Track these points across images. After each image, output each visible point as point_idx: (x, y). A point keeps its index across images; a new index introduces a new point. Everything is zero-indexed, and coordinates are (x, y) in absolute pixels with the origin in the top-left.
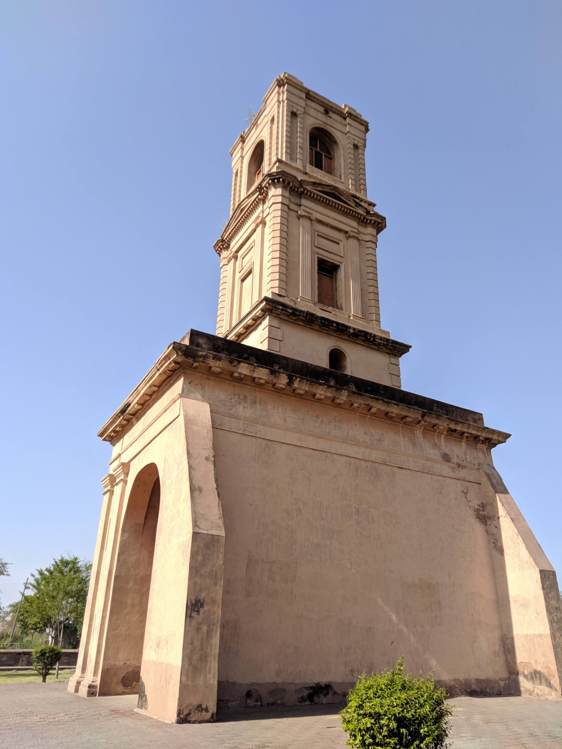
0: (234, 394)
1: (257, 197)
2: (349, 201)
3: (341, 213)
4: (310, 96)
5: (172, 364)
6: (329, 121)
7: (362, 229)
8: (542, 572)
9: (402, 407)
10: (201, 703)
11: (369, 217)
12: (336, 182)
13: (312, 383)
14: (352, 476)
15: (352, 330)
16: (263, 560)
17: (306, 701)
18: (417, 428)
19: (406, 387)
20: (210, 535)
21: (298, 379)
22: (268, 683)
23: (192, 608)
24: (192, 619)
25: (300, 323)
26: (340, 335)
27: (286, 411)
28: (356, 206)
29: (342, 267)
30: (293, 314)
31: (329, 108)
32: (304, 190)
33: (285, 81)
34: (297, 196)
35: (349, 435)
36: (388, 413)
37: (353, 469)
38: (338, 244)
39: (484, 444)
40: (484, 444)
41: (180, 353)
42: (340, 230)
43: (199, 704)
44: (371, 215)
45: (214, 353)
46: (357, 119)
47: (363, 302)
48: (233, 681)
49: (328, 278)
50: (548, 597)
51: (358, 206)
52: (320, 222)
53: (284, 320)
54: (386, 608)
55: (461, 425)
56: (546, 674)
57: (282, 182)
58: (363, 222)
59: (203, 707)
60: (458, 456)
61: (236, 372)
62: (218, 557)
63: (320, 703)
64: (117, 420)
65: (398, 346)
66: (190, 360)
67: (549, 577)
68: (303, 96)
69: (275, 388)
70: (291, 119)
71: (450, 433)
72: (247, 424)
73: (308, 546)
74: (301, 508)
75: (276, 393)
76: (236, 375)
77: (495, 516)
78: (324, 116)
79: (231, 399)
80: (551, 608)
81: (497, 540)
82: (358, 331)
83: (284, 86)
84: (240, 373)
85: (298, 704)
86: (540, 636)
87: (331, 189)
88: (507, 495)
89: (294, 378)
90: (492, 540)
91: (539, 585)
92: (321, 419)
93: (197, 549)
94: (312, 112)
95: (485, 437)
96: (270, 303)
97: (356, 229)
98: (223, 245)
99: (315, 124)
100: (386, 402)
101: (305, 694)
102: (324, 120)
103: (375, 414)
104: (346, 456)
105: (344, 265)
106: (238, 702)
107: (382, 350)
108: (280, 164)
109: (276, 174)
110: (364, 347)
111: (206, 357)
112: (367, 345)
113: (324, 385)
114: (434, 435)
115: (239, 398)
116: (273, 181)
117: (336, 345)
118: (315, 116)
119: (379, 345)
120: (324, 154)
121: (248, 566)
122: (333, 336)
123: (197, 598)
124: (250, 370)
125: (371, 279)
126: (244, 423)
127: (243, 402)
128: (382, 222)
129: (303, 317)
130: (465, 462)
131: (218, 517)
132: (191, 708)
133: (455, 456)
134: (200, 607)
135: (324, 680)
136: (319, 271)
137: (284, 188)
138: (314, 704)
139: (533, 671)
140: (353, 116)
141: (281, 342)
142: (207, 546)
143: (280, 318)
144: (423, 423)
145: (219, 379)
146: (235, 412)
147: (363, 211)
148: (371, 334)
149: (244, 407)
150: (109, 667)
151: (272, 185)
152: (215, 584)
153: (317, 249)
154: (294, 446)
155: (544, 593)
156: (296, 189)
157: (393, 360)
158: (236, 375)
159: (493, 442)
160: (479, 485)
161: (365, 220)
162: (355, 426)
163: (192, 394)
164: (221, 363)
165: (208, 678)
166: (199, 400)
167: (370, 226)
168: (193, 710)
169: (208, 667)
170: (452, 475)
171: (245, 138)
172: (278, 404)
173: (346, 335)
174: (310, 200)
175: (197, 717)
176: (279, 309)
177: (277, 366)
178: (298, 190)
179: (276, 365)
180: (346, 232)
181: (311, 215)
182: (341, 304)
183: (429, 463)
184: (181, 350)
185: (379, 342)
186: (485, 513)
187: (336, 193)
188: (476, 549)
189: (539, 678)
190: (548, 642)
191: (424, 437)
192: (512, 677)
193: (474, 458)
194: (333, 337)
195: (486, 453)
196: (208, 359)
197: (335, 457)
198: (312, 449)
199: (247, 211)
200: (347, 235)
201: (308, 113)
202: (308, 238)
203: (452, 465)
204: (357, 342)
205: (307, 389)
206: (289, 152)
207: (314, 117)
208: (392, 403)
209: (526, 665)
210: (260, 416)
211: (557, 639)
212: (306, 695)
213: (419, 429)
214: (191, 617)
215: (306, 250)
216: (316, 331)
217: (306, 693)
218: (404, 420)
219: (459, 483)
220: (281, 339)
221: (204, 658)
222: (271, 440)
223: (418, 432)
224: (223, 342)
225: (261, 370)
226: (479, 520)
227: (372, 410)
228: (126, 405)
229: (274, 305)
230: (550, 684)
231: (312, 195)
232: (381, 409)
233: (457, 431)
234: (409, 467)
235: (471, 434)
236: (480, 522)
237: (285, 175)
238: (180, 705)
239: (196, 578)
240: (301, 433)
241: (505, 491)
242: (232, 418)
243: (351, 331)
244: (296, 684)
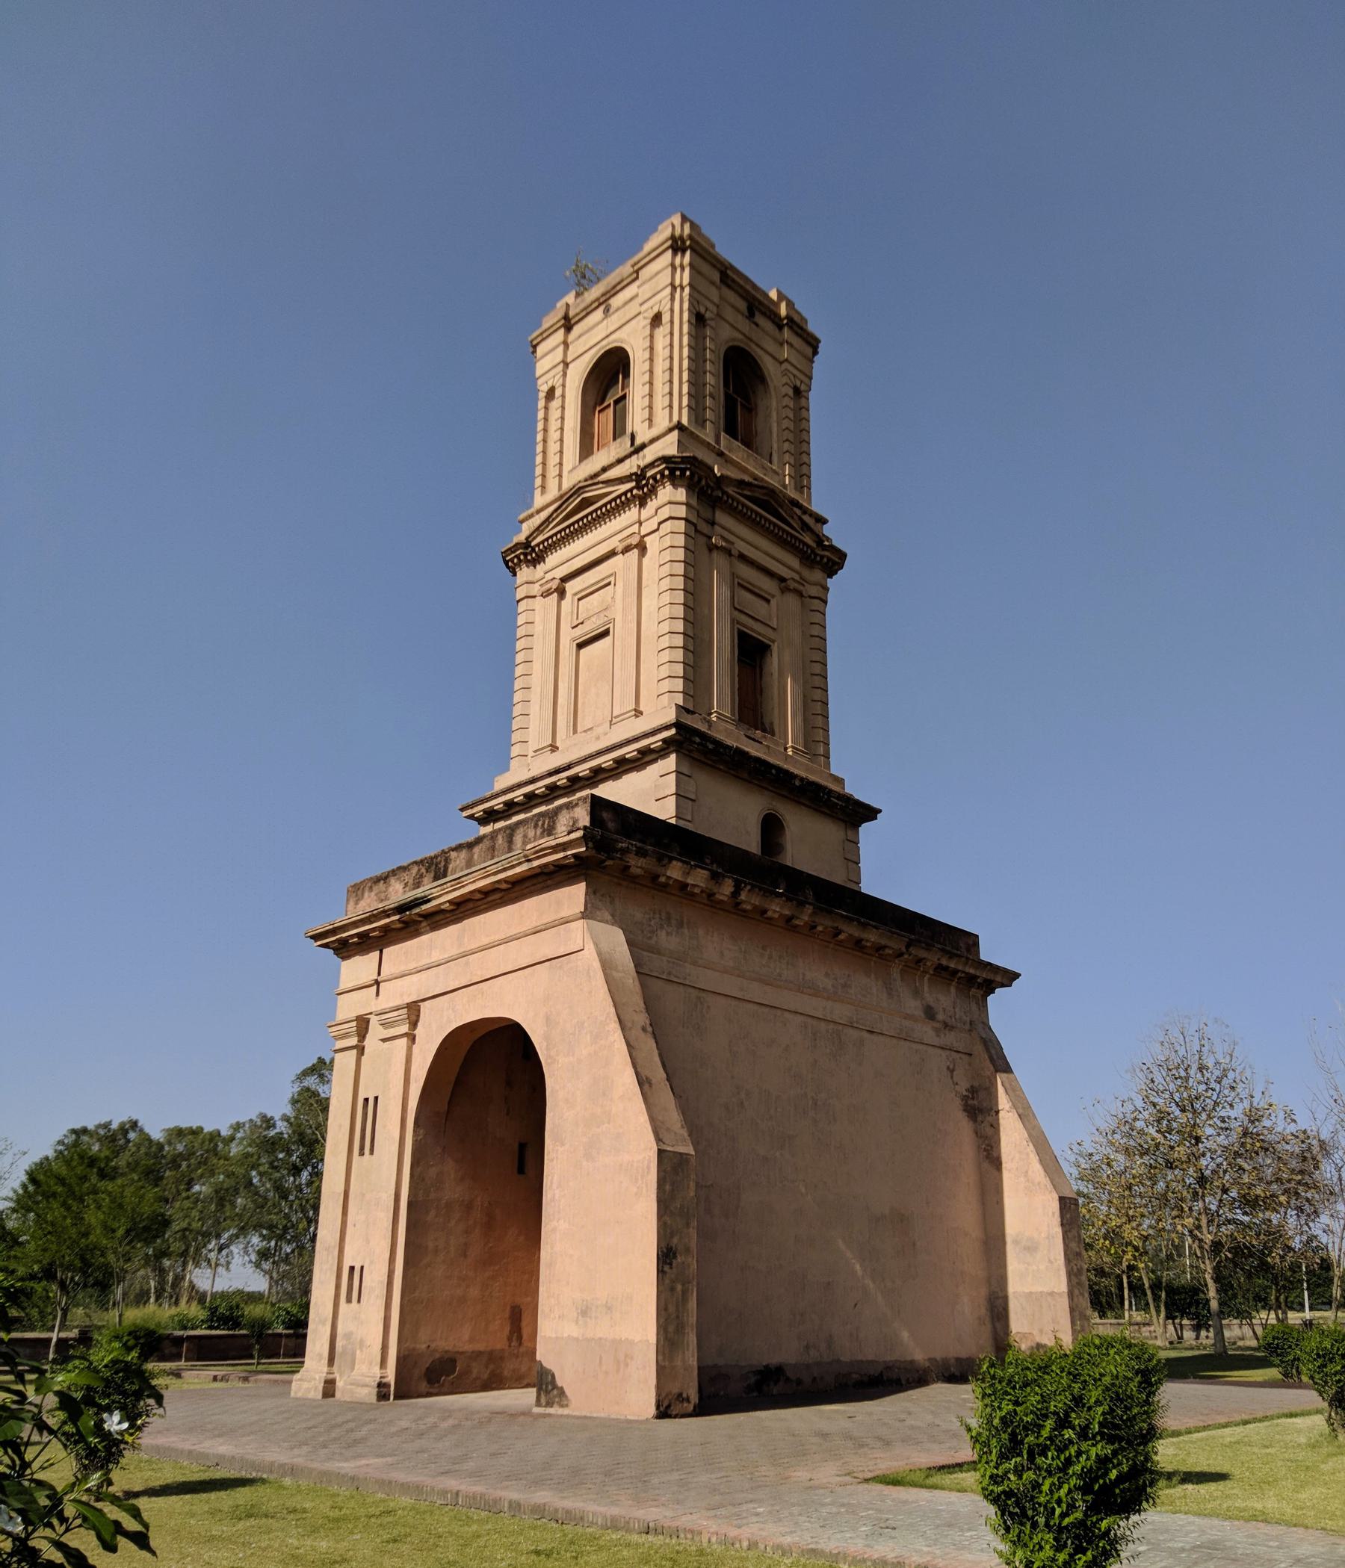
1: (631, 490)
2: (793, 518)
4: (728, 276)
5: (569, 859)
7: (806, 573)
8: (1061, 1199)
12: (765, 472)
19: (872, 885)
25: (721, 767)
29: (775, 648)
33: (688, 243)
38: (768, 601)
41: (590, 845)
45: (639, 844)
47: (805, 720)
52: (742, 557)
54: (849, 1254)
64: (380, 919)
68: (716, 277)
69: (712, 901)
70: (696, 330)
76: (663, 879)
77: (991, 1109)
78: (747, 321)
81: (992, 1147)
83: (684, 252)
84: (669, 878)
85: (744, 1395)
86: (1052, 1294)
87: (764, 494)
88: (1011, 1076)
90: (983, 1146)
91: (1057, 1219)
98: (525, 555)
99: (734, 340)
103: (841, 941)
105: (778, 647)
109: (679, 460)
116: (672, 471)
118: (732, 322)
124: (684, 872)
131: (680, 1126)
132: (670, 1397)
135: (774, 1360)
137: (690, 488)
139: (1034, 1345)
140: (796, 325)
144: (906, 956)
149: (668, 934)
150: (406, 1353)
152: (688, 1225)
158: (663, 879)
163: (598, 913)
170: (936, 1041)
171: (573, 322)
174: (730, 514)
176: (695, 743)
181: (732, 547)
182: (772, 724)
183: (907, 1023)
186: (975, 1102)
190: (1064, 1303)
191: (902, 980)
196: (628, 855)
197: (787, 1015)
199: (600, 508)
200: (783, 584)
202: (727, 593)
203: (937, 1025)
207: (732, 325)
209: (1025, 1336)
211: (1075, 1299)
214: (663, 1271)
217: (753, 1380)
218: (881, 952)
219: (944, 1054)
220: (693, 797)
221: (680, 1329)
228: (416, 899)
237: (697, 464)
238: (658, 1394)
241: (1007, 1069)
242: (652, 952)
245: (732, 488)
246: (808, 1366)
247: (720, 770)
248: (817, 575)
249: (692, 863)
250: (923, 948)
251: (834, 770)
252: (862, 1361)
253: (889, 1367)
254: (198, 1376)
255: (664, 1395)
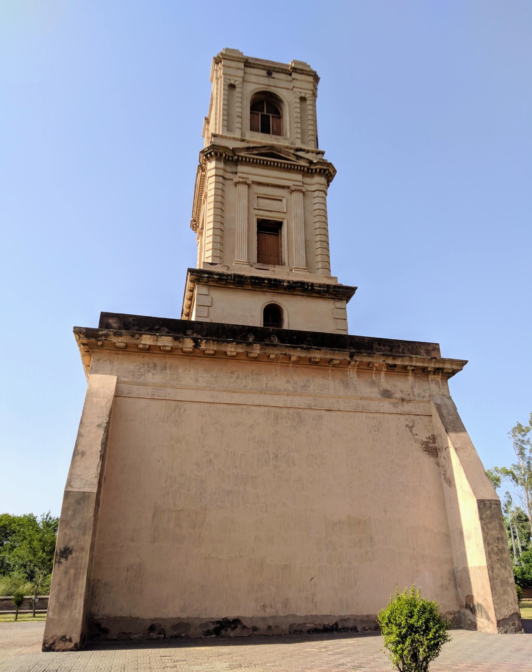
0: (144, 363)
2: (289, 156)
3: (282, 170)
4: (248, 63)
6: (272, 82)
7: (307, 180)
9: (325, 351)
10: (65, 634)
11: (313, 167)
12: (278, 140)
13: (219, 343)
14: (271, 424)
15: (286, 283)
16: (170, 509)
17: (211, 634)
18: (350, 368)
20: (81, 492)
21: (204, 341)
22: (172, 618)
23: (60, 555)
24: (60, 565)
26: (275, 290)
27: (198, 372)
28: (297, 159)
30: (220, 279)
31: (272, 69)
32: (238, 158)
34: (233, 165)
35: (268, 386)
36: (311, 359)
37: (272, 417)
38: (281, 200)
39: (437, 374)
40: (437, 374)
42: (283, 187)
43: (64, 635)
44: (315, 164)
46: (303, 72)
48: (137, 617)
49: (273, 236)
50: (487, 528)
51: (299, 158)
52: (259, 184)
53: (213, 286)
55: (400, 359)
56: (485, 607)
57: (214, 155)
58: (308, 172)
59: (67, 638)
60: (402, 391)
61: (140, 344)
62: (88, 511)
63: (227, 636)
65: (341, 290)
66: (93, 340)
67: (490, 507)
71: (389, 369)
72: (156, 389)
73: (219, 493)
74: (213, 459)
75: (187, 357)
76: (141, 346)
79: (140, 368)
80: (490, 538)
81: (446, 472)
82: (293, 283)
83: (221, 62)
85: (203, 637)
87: (268, 150)
89: (200, 340)
90: (442, 472)
92: (236, 374)
93: (68, 505)
94: (253, 79)
95: (435, 368)
96: (194, 274)
97: (300, 181)
100: (305, 349)
101: (211, 628)
102: (267, 83)
104: (264, 406)
105: (287, 220)
106: (141, 635)
107: (325, 296)
108: (215, 138)
109: (207, 149)
110: (304, 297)
111: (107, 335)
112: (307, 295)
113: (232, 343)
114: (372, 373)
115: (148, 367)
117: (271, 300)
119: (319, 292)
120: (271, 115)
121: (154, 516)
122: (268, 292)
123: (65, 546)
124: (154, 340)
125: (318, 228)
126: (153, 389)
127: (152, 369)
128: (329, 168)
129: (231, 280)
130: (411, 396)
131: (94, 476)
132: (55, 638)
133: (399, 391)
134: (69, 554)
135: (232, 615)
136: (259, 232)
137: (218, 160)
138: (220, 637)
141: (209, 308)
142: (78, 502)
143: (209, 286)
145: (127, 353)
146: (144, 380)
147: (305, 162)
148: (308, 283)
149: (153, 374)
151: (207, 160)
152: (84, 534)
153: (256, 211)
154: (206, 403)
155: (481, 524)
156: (231, 158)
157: (339, 304)
159: (446, 371)
160: (430, 417)
161: (310, 171)
162: (276, 376)
164: (123, 338)
165: (73, 613)
166: (107, 374)
167: (317, 175)
168: (57, 640)
169: (74, 604)
170: (394, 410)
172: (190, 367)
173: (283, 289)
174: (247, 165)
175: (60, 646)
177: (190, 332)
178: (232, 158)
179: (190, 330)
180: (288, 187)
183: (364, 402)
184: (82, 333)
185: (318, 289)
187: (275, 152)
188: (421, 482)
189: (480, 611)
191: (359, 376)
192: (462, 610)
193: (424, 391)
194: (268, 294)
195: (440, 382)
196: (110, 337)
197: (252, 408)
198: (226, 404)
201: (248, 80)
203: (394, 401)
204: (295, 293)
205: (215, 349)
206: (226, 124)
208: (312, 349)
210: (170, 380)
211: (496, 571)
212: (213, 628)
213: (352, 370)
215: (240, 216)
216: (249, 291)
217: (212, 627)
218: (331, 363)
219: (402, 418)
222: (181, 401)
223: (351, 372)
224: (134, 318)
225: (164, 339)
226: (427, 453)
227: (292, 359)
229: (199, 275)
230: (488, 616)
231: (248, 160)
232: (301, 356)
233: (397, 366)
234: (339, 408)
235: (415, 366)
236: (428, 454)
239: (66, 529)
240: (213, 390)
242: (140, 385)
243: (286, 284)
244: (202, 619)
245: (244, 153)
246: (264, 619)
247: (231, 288)
248: (217, 167)
249: (158, 334)
250: (365, 356)
251: (333, 274)
252: (317, 616)
253: (344, 620)
254: (79, 613)
255: (50, 636)
